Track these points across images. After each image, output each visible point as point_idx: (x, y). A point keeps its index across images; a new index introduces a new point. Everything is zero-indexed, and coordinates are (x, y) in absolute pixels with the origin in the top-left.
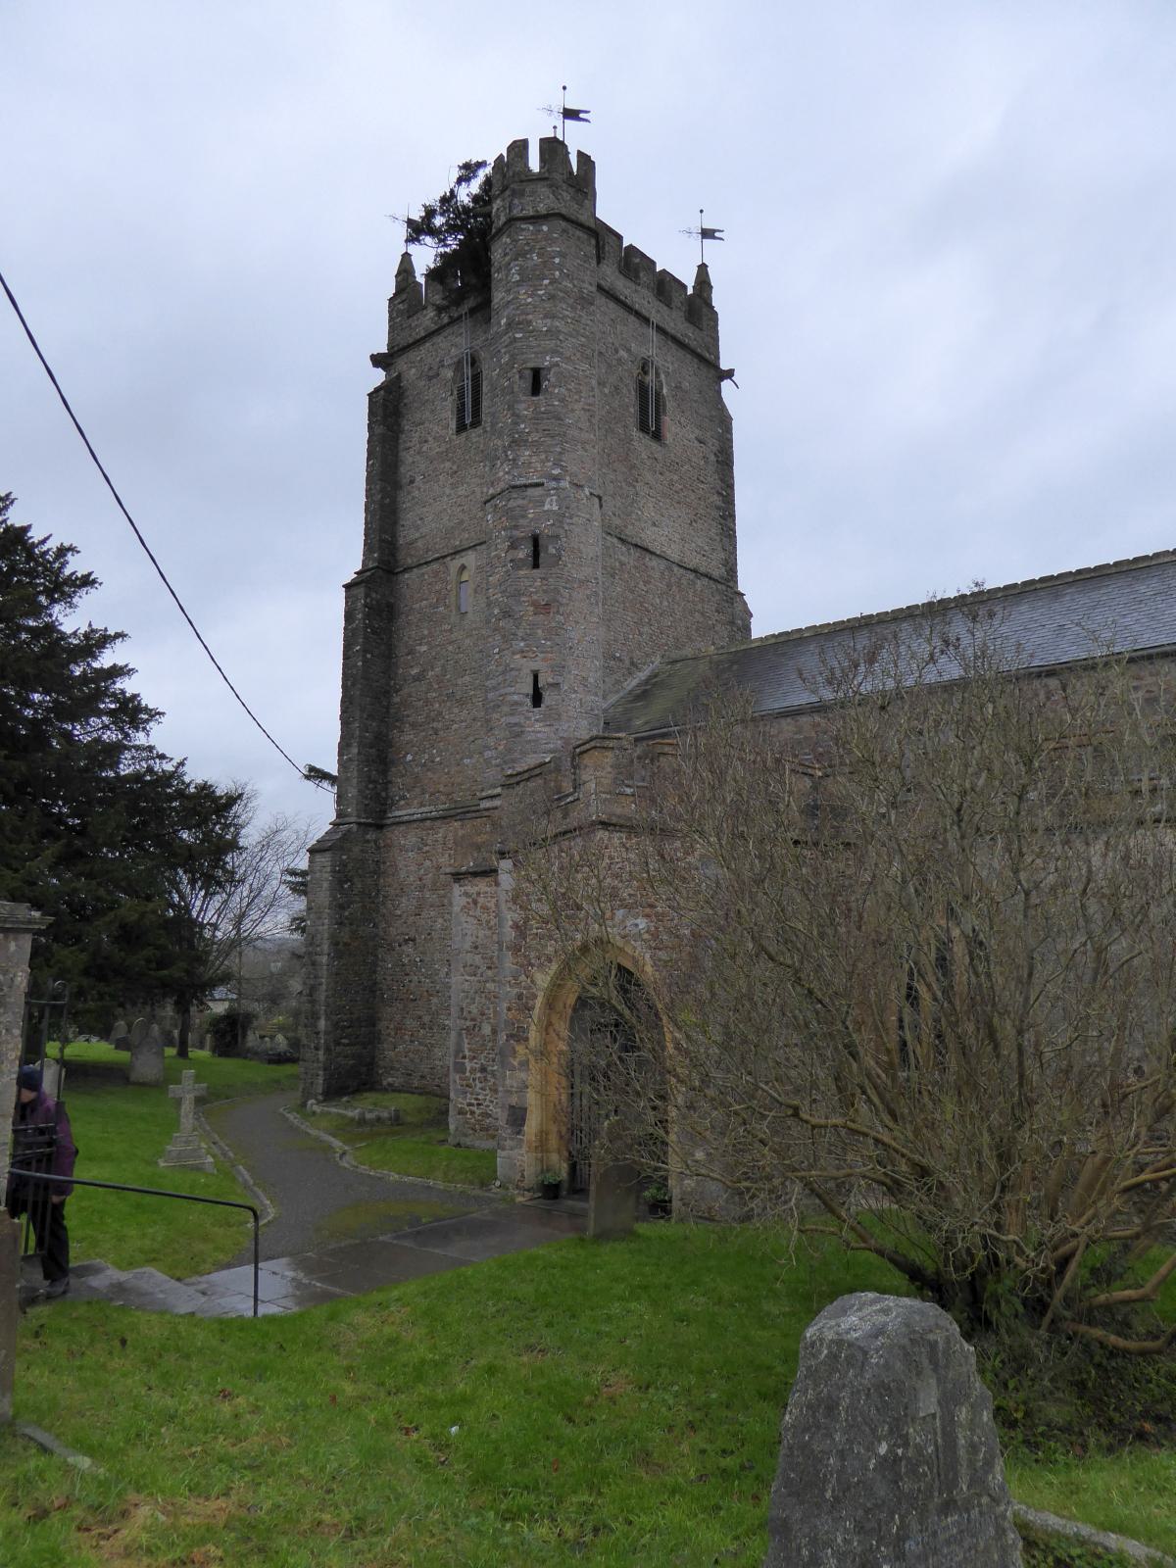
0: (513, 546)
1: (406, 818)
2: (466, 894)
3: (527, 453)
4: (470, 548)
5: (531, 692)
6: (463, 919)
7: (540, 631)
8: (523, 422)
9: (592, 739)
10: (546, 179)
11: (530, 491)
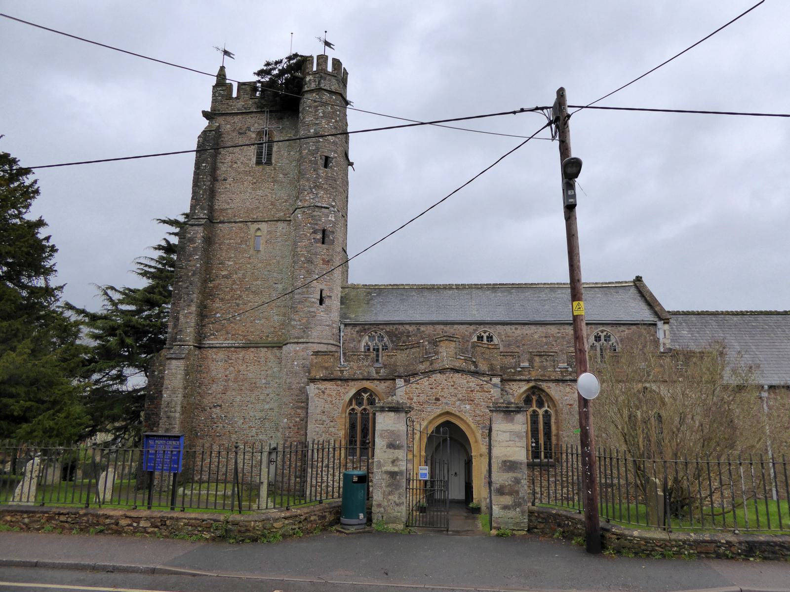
0: (315, 232)
1: (217, 345)
2: (318, 389)
4: (264, 221)
6: (317, 399)
10: (336, 76)
11: (323, 210)
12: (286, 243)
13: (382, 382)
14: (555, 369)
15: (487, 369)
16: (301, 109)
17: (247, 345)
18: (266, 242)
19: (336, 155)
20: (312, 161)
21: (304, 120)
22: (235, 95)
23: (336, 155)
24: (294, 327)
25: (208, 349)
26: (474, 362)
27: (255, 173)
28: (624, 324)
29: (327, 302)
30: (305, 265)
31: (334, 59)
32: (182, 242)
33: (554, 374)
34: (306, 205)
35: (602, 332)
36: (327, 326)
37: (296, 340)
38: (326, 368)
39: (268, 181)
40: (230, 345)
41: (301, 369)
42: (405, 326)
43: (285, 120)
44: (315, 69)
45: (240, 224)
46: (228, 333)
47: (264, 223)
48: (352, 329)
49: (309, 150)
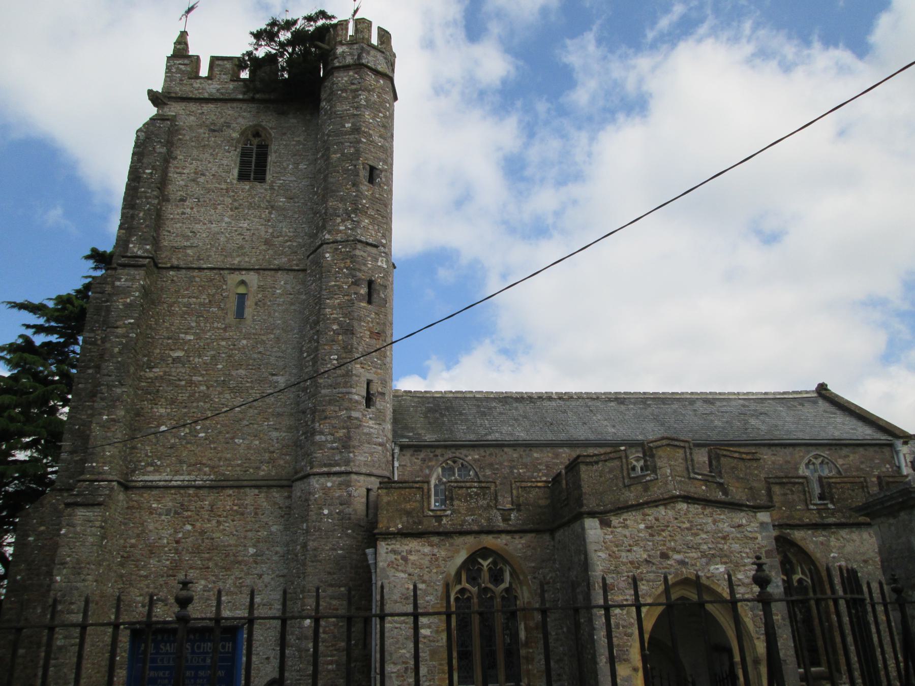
1: (161, 483)
3: (366, 221)
8: (364, 199)
9: (663, 438)
11: (369, 248)
12: (293, 307)
13: (517, 536)
14: (807, 505)
15: (744, 498)
16: (324, 96)
18: (256, 304)
19: (386, 167)
23: (386, 167)
24: (321, 445)
25: (142, 490)
26: (721, 485)
27: (236, 193)
28: (846, 445)
29: (379, 403)
30: (340, 337)
31: (379, 28)
33: (808, 514)
34: (339, 238)
35: (816, 458)
36: (380, 444)
37: (325, 469)
38: (408, 513)
39: (259, 206)
40: (186, 483)
42: (506, 449)
45: (208, 273)
46: (181, 462)
47: (252, 273)
48: (412, 455)
49: (343, 154)
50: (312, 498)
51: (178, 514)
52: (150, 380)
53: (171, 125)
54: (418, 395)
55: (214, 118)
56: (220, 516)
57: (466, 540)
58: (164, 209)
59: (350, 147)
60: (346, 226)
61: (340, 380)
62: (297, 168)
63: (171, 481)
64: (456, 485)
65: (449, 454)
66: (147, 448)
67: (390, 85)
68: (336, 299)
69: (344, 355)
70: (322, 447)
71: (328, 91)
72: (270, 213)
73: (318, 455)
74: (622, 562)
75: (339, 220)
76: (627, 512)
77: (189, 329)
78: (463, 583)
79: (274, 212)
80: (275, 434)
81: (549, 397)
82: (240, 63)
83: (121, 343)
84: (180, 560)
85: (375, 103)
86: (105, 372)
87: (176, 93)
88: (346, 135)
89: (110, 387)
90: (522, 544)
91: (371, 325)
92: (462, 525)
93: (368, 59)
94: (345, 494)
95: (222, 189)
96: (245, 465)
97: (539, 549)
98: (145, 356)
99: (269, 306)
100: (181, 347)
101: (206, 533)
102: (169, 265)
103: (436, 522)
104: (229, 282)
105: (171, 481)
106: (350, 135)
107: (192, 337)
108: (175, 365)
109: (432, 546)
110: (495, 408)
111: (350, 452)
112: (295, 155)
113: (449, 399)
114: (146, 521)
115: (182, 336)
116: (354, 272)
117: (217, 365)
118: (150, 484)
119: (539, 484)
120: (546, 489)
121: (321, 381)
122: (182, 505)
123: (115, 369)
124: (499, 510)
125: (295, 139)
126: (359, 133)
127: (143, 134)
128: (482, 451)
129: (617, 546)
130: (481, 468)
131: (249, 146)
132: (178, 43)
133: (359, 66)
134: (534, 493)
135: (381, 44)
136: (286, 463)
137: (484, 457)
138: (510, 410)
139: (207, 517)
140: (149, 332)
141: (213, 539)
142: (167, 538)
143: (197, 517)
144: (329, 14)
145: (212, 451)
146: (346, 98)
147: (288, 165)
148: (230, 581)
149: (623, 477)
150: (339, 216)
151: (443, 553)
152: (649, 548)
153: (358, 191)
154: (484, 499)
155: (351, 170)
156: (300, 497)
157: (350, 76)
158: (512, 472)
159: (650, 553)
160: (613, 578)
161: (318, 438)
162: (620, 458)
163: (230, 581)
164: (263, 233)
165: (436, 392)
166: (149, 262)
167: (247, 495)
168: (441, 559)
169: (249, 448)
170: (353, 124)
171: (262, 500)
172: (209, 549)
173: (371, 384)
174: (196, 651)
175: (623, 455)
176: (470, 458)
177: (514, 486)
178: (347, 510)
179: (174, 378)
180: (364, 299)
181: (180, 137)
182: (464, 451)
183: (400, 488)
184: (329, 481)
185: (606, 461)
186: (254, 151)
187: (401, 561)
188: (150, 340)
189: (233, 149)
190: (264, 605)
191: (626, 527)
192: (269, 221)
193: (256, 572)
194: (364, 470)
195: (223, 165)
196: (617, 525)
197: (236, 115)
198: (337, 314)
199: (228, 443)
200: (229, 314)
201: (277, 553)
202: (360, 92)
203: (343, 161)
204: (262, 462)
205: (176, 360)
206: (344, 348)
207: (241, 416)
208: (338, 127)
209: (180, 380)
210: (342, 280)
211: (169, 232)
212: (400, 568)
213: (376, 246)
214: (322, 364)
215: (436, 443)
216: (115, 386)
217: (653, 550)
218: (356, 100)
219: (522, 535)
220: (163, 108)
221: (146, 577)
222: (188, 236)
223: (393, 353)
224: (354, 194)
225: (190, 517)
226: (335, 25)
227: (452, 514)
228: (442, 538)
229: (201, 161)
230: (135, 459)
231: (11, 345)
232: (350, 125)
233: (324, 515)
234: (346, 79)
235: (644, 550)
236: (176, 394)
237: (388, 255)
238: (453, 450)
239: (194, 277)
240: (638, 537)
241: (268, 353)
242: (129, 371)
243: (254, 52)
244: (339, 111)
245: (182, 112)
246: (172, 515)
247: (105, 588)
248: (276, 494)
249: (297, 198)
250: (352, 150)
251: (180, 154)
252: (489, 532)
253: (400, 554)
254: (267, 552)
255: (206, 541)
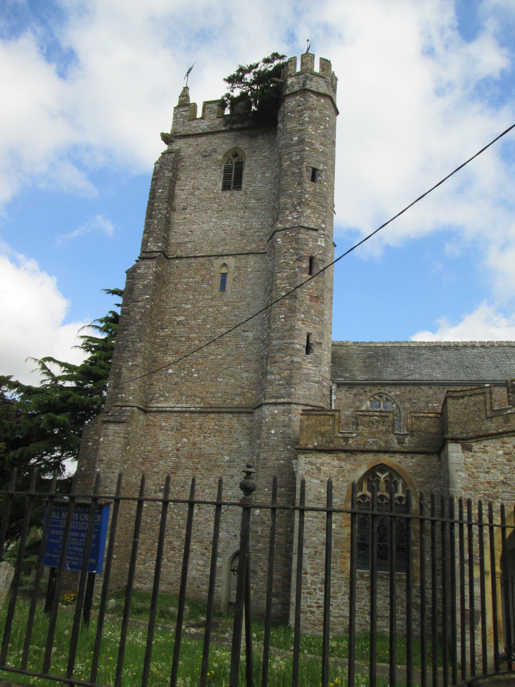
1: (168, 409)
3: (309, 211)
5: (306, 345)
7: (313, 311)
10: (324, 78)
11: (310, 232)
12: (260, 281)
13: (409, 456)
16: (279, 119)
17: (206, 410)
18: (234, 280)
19: (326, 168)
20: (295, 173)
21: (285, 128)
22: (199, 115)
23: (326, 168)
24: (271, 383)
25: (156, 414)
29: (316, 350)
31: (322, 59)
32: (130, 282)
34: (287, 226)
36: (316, 382)
37: (273, 400)
38: (323, 435)
40: (184, 409)
41: (280, 439)
42: (422, 387)
43: (259, 138)
44: (298, 69)
45: (201, 259)
46: (182, 394)
47: (231, 257)
48: (347, 391)
49: (292, 161)
50: (264, 421)
51: (179, 430)
52: (162, 338)
53: (176, 156)
54: (364, 345)
55: (206, 147)
56: (206, 433)
57: (367, 458)
58: (172, 216)
59: (297, 155)
60: (293, 216)
61: (285, 333)
62: (264, 176)
63: (174, 407)
64: (361, 413)
65: (376, 390)
66: (160, 384)
67: (330, 103)
68: (285, 272)
69: (289, 315)
70: (272, 384)
71: (282, 114)
72: (244, 212)
73: (269, 390)
74: (480, 481)
75: (288, 212)
76: (487, 439)
77: (188, 300)
78: (364, 490)
79: (246, 211)
80: (245, 375)
81: (473, 346)
82: (222, 104)
83: (141, 312)
84: (179, 462)
85: (316, 119)
86: (131, 332)
87: (180, 133)
88: (293, 147)
89: (133, 342)
90: (413, 462)
91: (311, 291)
92: (364, 445)
93: (311, 85)
94: (287, 419)
95: (211, 198)
96: (224, 397)
97: (427, 468)
98: (159, 321)
99: (243, 281)
100: (183, 313)
101: (196, 444)
102: (175, 256)
103: (344, 441)
104: (215, 265)
105: (174, 407)
106: (297, 146)
107: (190, 306)
108: (179, 326)
109: (340, 460)
110: (423, 354)
111: (292, 388)
112: (262, 167)
113: (387, 348)
114: (158, 435)
115: (183, 305)
116: (297, 251)
117: (206, 325)
118: (160, 409)
119: (431, 415)
120: (436, 419)
121: (272, 334)
122: (181, 424)
123: (137, 330)
124: (395, 434)
125: (263, 155)
126: (303, 144)
127: (159, 165)
128: (403, 388)
129: (476, 468)
130: (401, 402)
131: (230, 164)
132: (182, 96)
133: (304, 91)
134: (426, 422)
135: (322, 71)
136: (252, 396)
137: (405, 393)
138: (436, 356)
139: (197, 433)
140: (162, 304)
141: (201, 449)
142: (171, 447)
143: (191, 433)
144: (280, 54)
145: (202, 387)
146: (295, 118)
147: (257, 175)
148: (212, 479)
149: (486, 410)
150: (288, 209)
151: (348, 466)
152: (506, 472)
153: (302, 188)
154: (383, 425)
155: (297, 173)
156: (257, 420)
157: (297, 100)
158: (427, 406)
159: (506, 476)
160: (471, 494)
161: (269, 377)
162: (484, 393)
163: (212, 479)
164: (239, 227)
165: (379, 343)
166: (160, 255)
167: (224, 419)
168: (346, 470)
169: (227, 384)
170: (299, 137)
171: (235, 422)
172: (198, 456)
173: (310, 336)
174: (81, 519)
175: (487, 390)
176: (393, 393)
177: (409, 415)
178: (288, 431)
179: (178, 336)
180: (305, 271)
181: (183, 164)
182: (388, 389)
183: (317, 415)
184: (276, 409)
185: (470, 396)
186: (234, 167)
187: (315, 470)
188: (162, 310)
189: (219, 167)
190: (234, 497)
191: (486, 452)
192: (243, 218)
193: (229, 474)
194: (302, 402)
195: (211, 180)
196: (477, 450)
197: (221, 142)
198: (285, 284)
199: (213, 381)
200: (215, 288)
201: (244, 461)
202: (304, 112)
203: (292, 166)
204: (236, 395)
205: (179, 323)
206: (290, 309)
207: (222, 361)
208: (288, 141)
209: (182, 337)
210: (289, 258)
211: (176, 232)
212: (314, 476)
213: (316, 230)
214: (274, 322)
215: (365, 382)
216: (137, 342)
217: (509, 473)
218: (302, 118)
219: (413, 455)
220: (171, 145)
221: (157, 473)
222: (188, 234)
223: (333, 312)
224: (299, 191)
225: (186, 433)
226: (287, 63)
227: (357, 436)
228: (348, 454)
229: (197, 179)
230: (152, 392)
231: (105, 318)
232: (297, 138)
233: (272, 434)
234: (294, 103)
235: (501, 473)
236: (179, 347)
237: (328, 237)
238: (379, 388)
239: (192, 263)
240: (496, 461)
241: (241, 315)
242: (145, 332)
243: (231, 94)
244: (289, 128)
245: (184, 146)
246: (175, 431)
247: (130, 478)
248: (244, 418)
249: (264, 199)
250: (298, 158)
251: (182, 176)
252: (386, 452)
253: (315, 465)
254: (237, 460)
255: (196, 450)
